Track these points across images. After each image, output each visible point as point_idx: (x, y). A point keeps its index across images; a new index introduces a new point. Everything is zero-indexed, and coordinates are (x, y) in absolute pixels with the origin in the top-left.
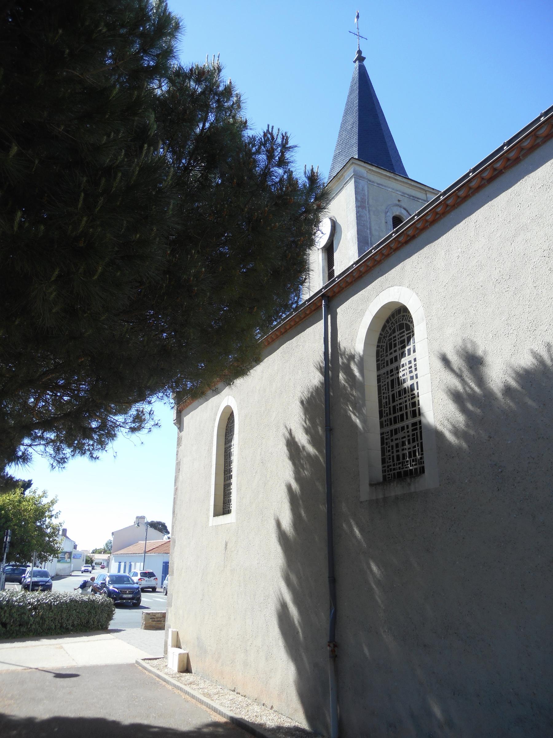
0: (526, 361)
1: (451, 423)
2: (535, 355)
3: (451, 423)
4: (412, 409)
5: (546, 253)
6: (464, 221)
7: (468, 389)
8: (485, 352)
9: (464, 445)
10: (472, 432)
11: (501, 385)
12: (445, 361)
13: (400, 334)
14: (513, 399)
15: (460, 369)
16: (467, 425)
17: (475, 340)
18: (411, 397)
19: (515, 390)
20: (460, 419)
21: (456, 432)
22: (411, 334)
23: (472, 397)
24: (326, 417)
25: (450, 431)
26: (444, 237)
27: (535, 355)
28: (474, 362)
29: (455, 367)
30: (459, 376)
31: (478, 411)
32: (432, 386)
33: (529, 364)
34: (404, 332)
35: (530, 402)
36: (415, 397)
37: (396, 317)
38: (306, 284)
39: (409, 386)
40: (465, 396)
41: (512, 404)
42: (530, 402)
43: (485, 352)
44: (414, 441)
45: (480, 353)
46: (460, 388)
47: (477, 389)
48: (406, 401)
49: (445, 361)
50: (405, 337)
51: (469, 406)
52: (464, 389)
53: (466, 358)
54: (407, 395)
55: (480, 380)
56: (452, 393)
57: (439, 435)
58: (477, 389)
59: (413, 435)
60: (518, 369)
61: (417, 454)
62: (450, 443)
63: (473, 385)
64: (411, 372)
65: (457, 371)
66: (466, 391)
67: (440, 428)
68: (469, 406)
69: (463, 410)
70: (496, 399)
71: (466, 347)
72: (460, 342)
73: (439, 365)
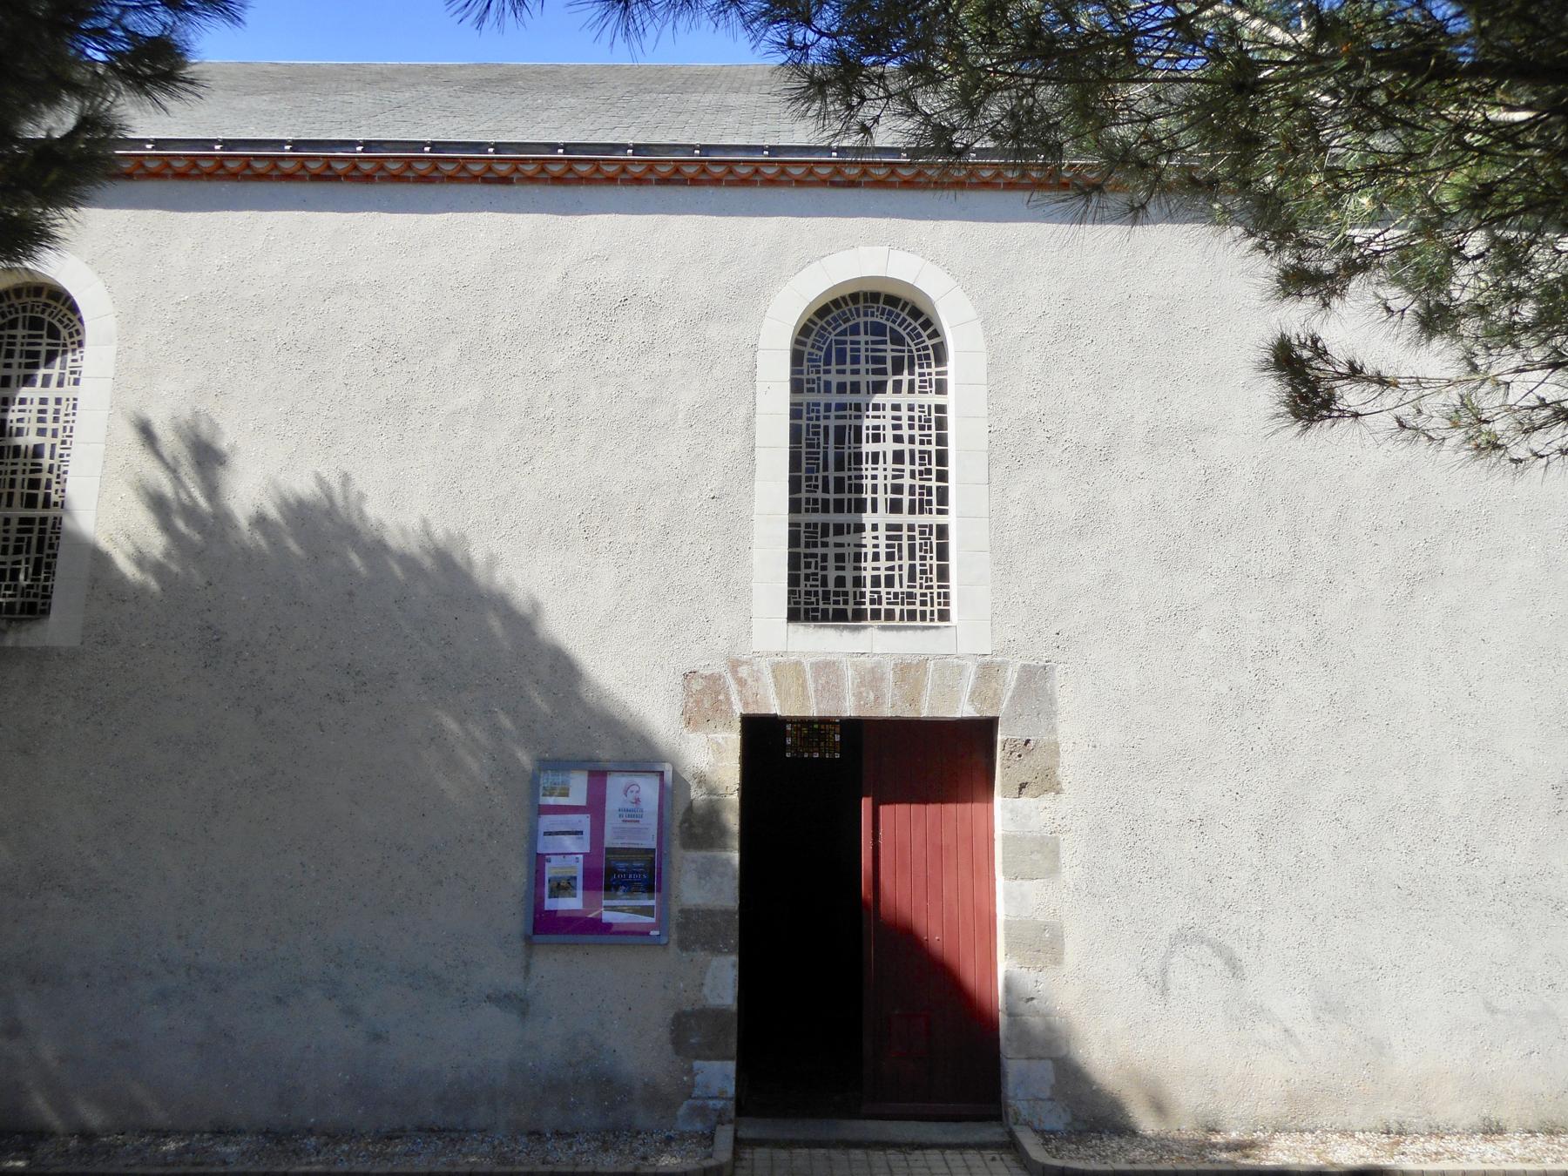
0: (303, 485)
1: (134, 544)
2: (320, 480)
3: (134, 544)
4: (26, 491)
5: (375, 344)
6: (247, 214)
7: (184, 496)
8: (233, 448)
9: (154, 585)
10: (175, 568)
11: (252, 511)
12: (146, 433)
13: (30, 336)
14: (266, 534)
15: (174, 458)
16: (167, 555)
17: (218, 421)
18: (30, 467)
19: (273, 524)
20: (156, 543)
21: (140, 560)
22: (61, 349)
23: (190, 513)
24: (921, 1119)
25: (129, 557)
26: (199, 215)
27: (320, 480)
28: (207, 457)
29: (166, 453)
30: (172, 470)
31: (197, 537)
32: (104, 467)
33: (308, 491)
34: (41, 337)
35: (293, 546)
36: (40, 471)
37: (24, 299)
38: (744, 1163)
39: (31, 447)
40: (175, 506)
41: (263, 543)
42: (293, 546)
43: (233, 448)
44: (18, 550)
45: (223, 444)
46: (167, 488)
47: (203, 502)
48: (14, 472)
49: (146, 433)
50: (43, 349)
51: (180, 524)
52: (177, 493)
53: (194, 444)
54: (21, 460)
55: (212, 491)
56: (148, 493)
57: (99, 559)
58: (203, 502)
59: (19, 540)
60: (287, 494)
61: (22, 577)
62: (122, 578)
63: (197, 493)
64: (41, 420)
65: (169, 460)
66: (179, 499)
67: (104, 544)
68: (180, 524)
69: (166, 526)
70: (236, 527)
71: (197, 426)
72: (186, 413)
73: (131, 436)
